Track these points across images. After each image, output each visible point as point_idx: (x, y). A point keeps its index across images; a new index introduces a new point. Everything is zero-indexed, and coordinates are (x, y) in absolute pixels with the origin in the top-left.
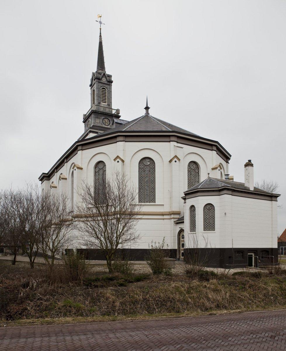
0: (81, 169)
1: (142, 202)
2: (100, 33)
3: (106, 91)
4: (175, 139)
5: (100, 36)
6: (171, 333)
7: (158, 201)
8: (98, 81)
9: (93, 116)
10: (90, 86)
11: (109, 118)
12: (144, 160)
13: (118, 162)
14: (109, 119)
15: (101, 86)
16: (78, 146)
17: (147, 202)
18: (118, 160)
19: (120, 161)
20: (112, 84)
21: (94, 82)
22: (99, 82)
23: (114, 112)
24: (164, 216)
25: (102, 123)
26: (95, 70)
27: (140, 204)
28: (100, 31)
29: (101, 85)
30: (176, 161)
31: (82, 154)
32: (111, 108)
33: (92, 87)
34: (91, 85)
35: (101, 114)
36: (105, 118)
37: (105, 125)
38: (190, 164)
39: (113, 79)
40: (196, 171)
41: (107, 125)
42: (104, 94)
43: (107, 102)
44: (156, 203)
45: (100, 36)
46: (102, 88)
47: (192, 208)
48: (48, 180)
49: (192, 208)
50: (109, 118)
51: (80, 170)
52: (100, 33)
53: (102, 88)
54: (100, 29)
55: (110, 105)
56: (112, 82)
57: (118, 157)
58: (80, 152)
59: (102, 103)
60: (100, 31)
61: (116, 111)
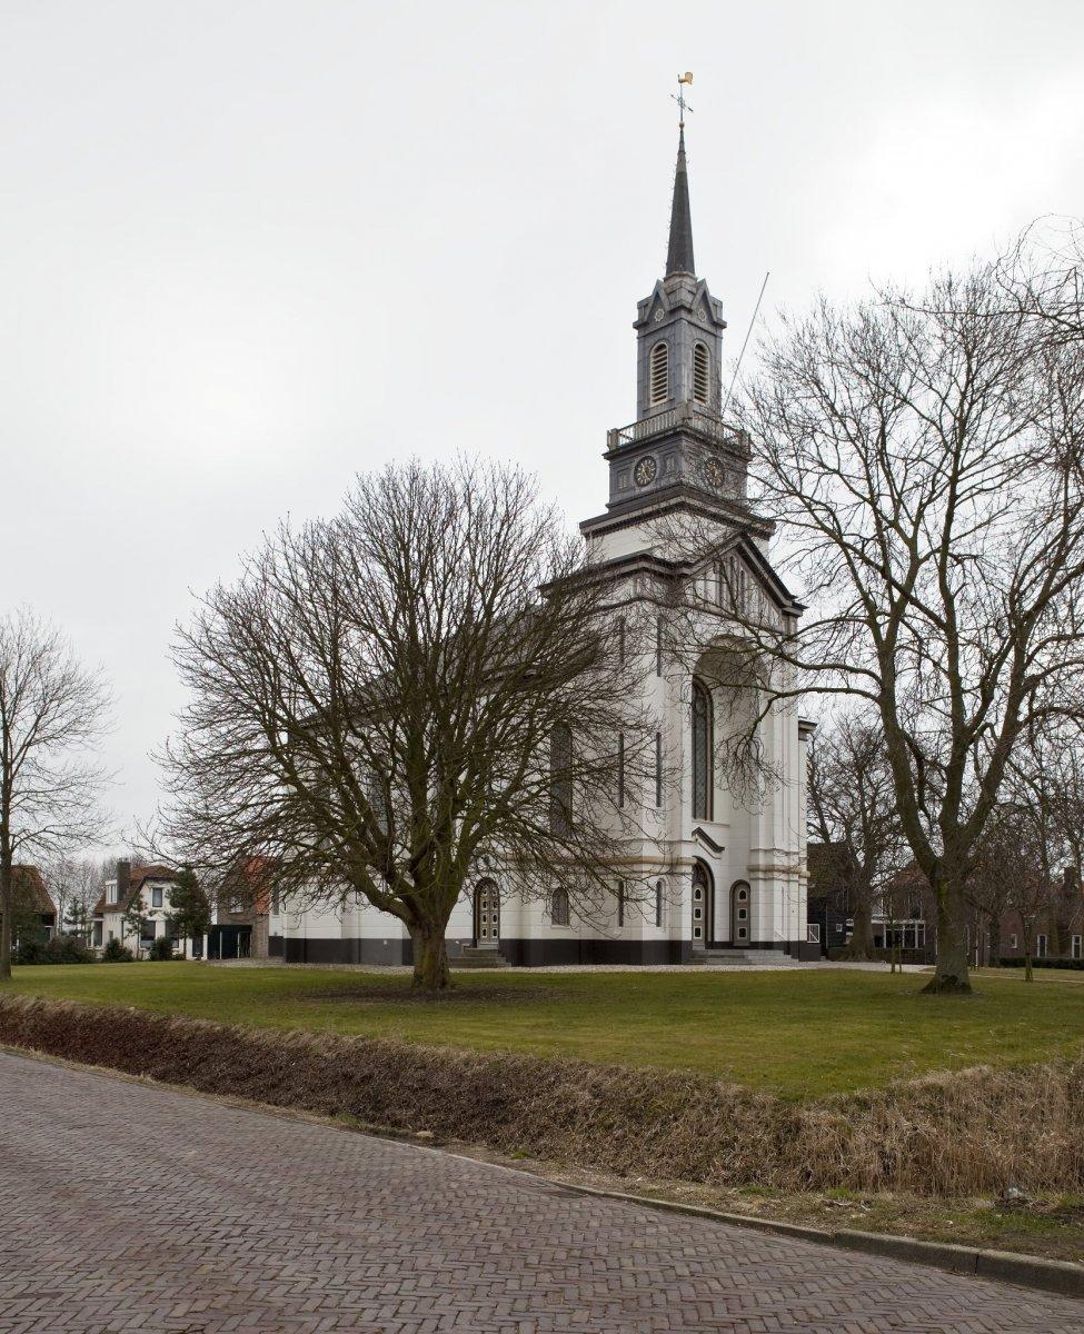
2: (682, 142)
5: (682, 152)
45: (682, 152)
52: (682, 142)
54: (682, 126)
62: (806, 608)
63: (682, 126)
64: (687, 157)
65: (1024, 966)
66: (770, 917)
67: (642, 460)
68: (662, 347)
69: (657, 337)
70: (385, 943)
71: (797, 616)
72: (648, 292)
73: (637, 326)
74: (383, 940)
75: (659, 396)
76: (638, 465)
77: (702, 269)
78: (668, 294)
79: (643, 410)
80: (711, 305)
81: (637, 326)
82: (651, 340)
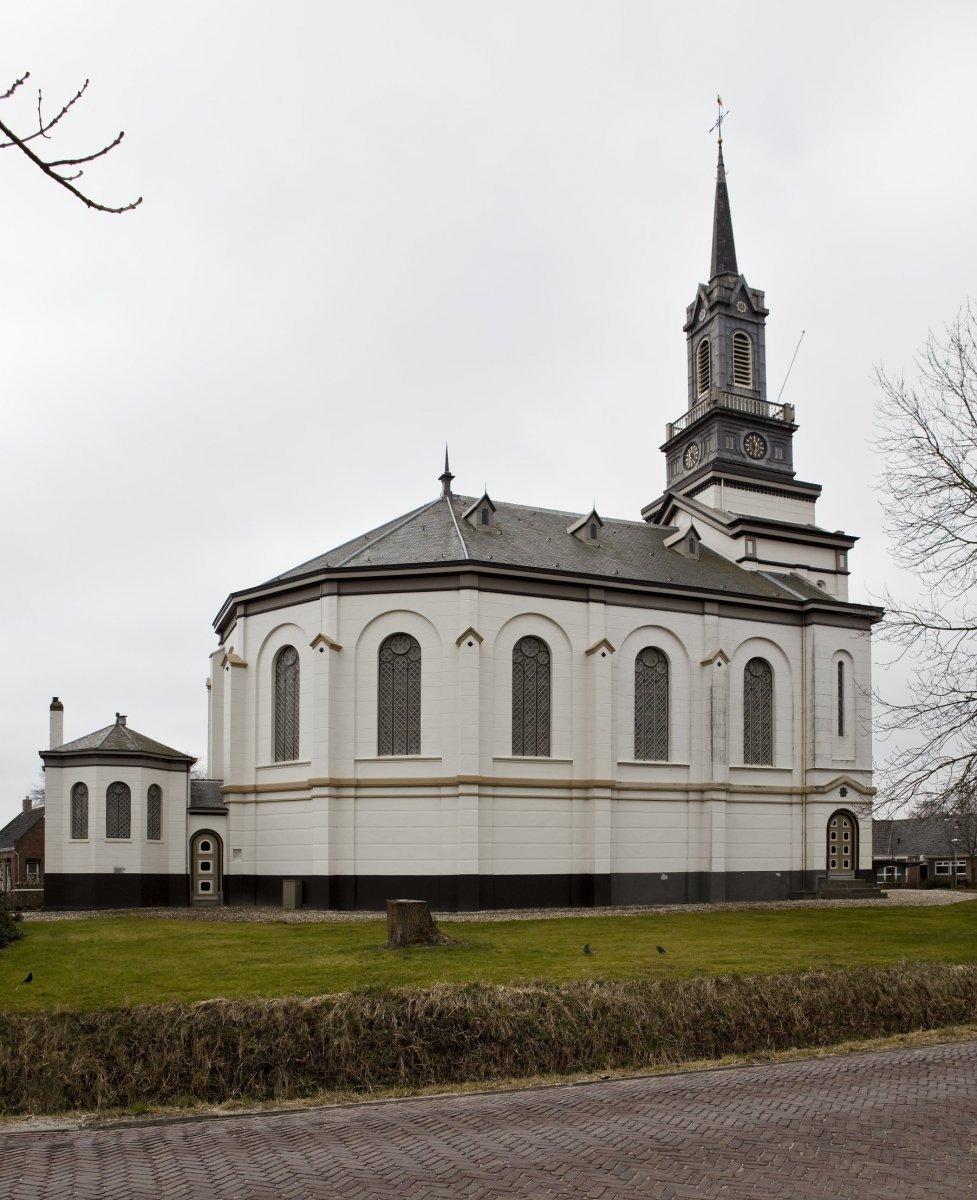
0: (244, 666)
1: (386, 753)
2: (721, 157)
3: (747, 344)
4: (474, 581)
5: (721, 165)
6: (651, 1137)
7: (427, 748)
8: (723, 311)
9: (716, 427)
10: (685, 331)
11: (764, 435)
12: (394, 642)
13: (322, 650)
14: (766, 438)
15: (734, 327)
16: (237, 604)
17: (400, 751)
18: (322, 645)
19: (327, 649)
20: (767, 319)
21: (703, 316)
22: (726, 316)
23: (772, 411)
24: (442, 789)
25: (744, 452)
26: (704, 275)
27: (381, 757)
28: (720, 147)
29: (734, 324)
30: (470, 644)
31: (245, 626)
32: (762, 399)
33: (697, 333)
34: (688, 329)
35: (739, 419)
36: (752, 434)
37: (752, 457)
38: (523, 644)
39: (767, 304)
40: (540, 660)
41: (757, 459)
42: (741, 357)
43: (751, 381)
44: (422, 756)
45: (721, 165)
46: (738, 336)
47: (79, 790)
48: (801, 626)
49: (79, 790)
50: (764, 435)
51: (239, 670)
52: (721, 157)
53: (738, 336)
54: (720, 142)
55: (759, 393)
56: (765, 314)
57: (320, 638)
58: (240, 621)
59: (736, 384)
60: (720, 147)
61: (778, 409)
62: (857, 539)
63: (720, 142)
64: (726, 168)
65: (228, 878)
66: (228, 865)
67: (752, 434)
68: (706, 342)
69: (701, 335)
70: (664, 877)
71: (847, 549)
72: (693, 298)
73: (687, 329)
74: (659, 875)
75: (705, 387)
76: (686, 452)
77: (743, 268)
78: (732, 290)
79: (694, 402)
80: (750, 295)
81: (687, 329)
82: (697, 339)
